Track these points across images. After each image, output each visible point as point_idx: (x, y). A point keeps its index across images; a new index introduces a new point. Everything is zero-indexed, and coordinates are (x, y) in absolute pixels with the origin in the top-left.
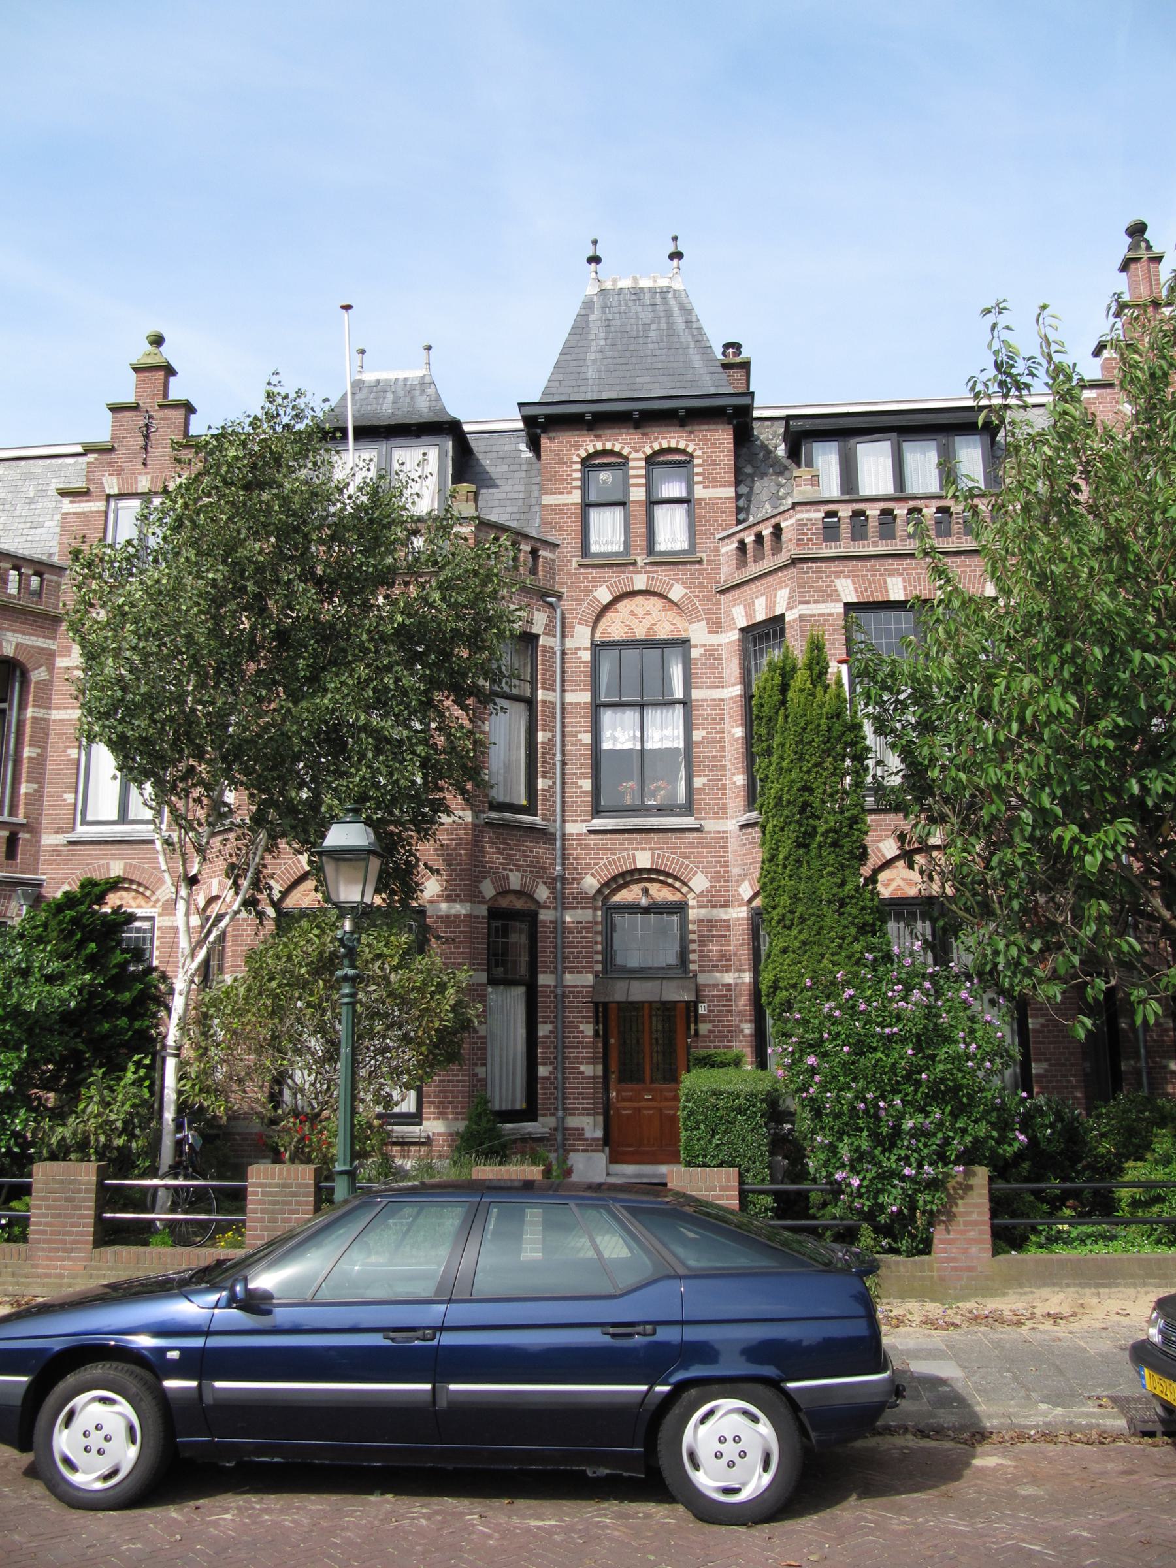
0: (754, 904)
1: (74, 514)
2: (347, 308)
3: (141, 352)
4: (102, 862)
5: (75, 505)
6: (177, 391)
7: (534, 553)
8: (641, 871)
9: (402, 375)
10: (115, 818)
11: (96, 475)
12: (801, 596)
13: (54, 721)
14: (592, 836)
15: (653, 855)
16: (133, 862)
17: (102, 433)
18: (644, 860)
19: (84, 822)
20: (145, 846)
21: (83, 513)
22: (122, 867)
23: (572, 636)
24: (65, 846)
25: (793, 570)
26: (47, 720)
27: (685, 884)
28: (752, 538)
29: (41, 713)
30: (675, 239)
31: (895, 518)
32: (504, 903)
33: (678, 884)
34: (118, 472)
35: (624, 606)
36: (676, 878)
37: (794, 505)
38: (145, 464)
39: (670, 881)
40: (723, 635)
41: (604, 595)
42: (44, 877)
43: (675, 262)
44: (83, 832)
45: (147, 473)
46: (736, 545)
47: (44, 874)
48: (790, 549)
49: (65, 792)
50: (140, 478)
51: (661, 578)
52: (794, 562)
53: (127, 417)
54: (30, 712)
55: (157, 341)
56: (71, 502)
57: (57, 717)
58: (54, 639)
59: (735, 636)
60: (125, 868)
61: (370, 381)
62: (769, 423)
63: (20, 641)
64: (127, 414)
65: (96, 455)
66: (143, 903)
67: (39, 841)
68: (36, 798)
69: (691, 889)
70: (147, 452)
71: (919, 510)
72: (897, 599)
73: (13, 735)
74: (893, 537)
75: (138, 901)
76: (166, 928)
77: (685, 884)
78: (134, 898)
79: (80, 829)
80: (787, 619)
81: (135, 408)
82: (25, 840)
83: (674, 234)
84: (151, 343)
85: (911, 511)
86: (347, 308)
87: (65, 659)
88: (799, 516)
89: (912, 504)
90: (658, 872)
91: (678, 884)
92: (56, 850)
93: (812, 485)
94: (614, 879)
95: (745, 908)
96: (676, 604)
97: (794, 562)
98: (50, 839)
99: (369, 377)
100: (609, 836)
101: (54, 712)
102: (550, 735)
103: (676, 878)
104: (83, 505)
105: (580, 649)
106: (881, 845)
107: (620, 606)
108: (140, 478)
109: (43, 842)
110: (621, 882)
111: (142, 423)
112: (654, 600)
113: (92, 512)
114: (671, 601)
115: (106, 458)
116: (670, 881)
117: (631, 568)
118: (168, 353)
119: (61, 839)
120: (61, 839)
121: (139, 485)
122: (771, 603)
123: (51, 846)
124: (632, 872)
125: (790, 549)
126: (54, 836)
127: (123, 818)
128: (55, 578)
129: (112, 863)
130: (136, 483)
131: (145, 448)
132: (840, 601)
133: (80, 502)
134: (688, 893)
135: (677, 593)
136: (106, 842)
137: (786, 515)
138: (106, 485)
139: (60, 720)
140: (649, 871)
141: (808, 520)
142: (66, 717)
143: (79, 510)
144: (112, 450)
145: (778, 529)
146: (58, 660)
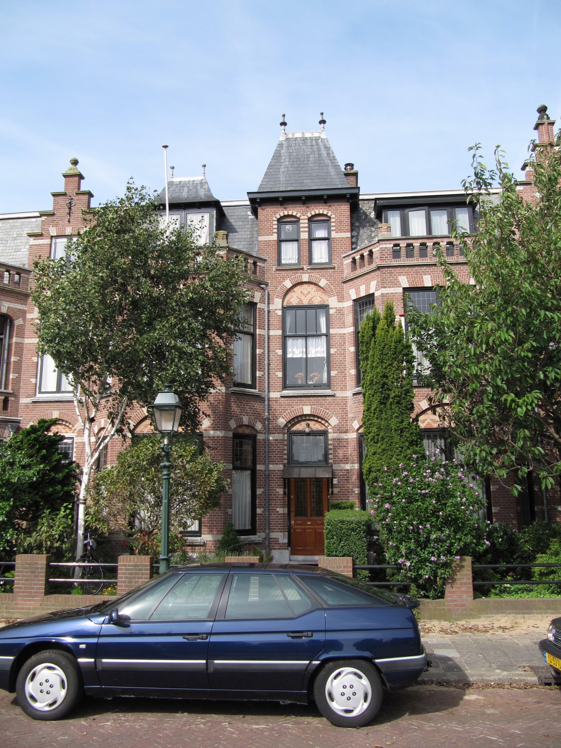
0: (360, 431)
1: (35, 245)
2: (166, 147)
3: (67, 168)
4: (49, 411)
5: (36, 241)
6: (84, 187)
7: (255, 264)
8: (306, 415)
9: (192, 179)
10: (55, 390)
11: (46, 227)
12: (382, 284)
13: (26, 344)
14: (283, 399)
15: (312, 408)
16: (63, 411)
17: (49, 207)
18: (307, 410)
19: (40, 392)
20: (69, 404)
21: (40, 245)
22: (58, 413)
23: (273, 304)
24: (31, 403)
25: (378, 272)
26: (22, 344)
27: (327, 422)
28: (359, 257)
29: (20, 340)
30: (322, 114)
31: (427, 247)
32: (240, 431)
33: (323, 422)
34: (56, 225)
35: (298, 289)
36: (323, 419)
37: (379, 241)
38: (69, 221)
39: (319, 420)
40: (345, 303)
41: (288, 284)
42: (21, 418)
43: (322, 125)
44: (40, 397)
45: (70, 226)
46: (351, 260)
47: (21, 417)
48: (377, 262)
49: (31, 378)
50: (67, 228)
51: (315, 276)
52: (379, 268)
53: (61, 199)
54: (14, 340)
55: (75, 162)
56: (34, 239)
57: (27, 342)
58: (26, 305)
59: (351, 303)
60: (60, 414)
61: (177, 182)
62: (367, 202)
63: (10, 306)
64: (61, 197)
65: (46, 217)
66: (68, 431)
67: (18, 401)
68: (17, 381)
69: (330, 424)
70: (70, 216)
71: (439, 243)
72: (428, 286)
73: (6, 351)
74: (426, 256)
75: (66, 430)
76: (79, 442)
77: (327, 422)
78: (64, 428)
79: (38, 395)
80: (375, 295)
81: (65, 194)
82: (12, 401)
83: (321, 112)
84: (72, 164)
85: (435, 244)
86: (166, 147)
87: (31, 315)
88: (381, 246)
89: (435, 240)
90: (314, 416)
91: (323, 422)
92: (27, 405)
93: (387, 231)
94: (293, 419)
95: (355, 433)
96: (322, 288)
97: (379, 268)
98: (24, 400)
99: (176, 180)
100: (290, 399)
101: (26, 340)
102: (262, 351)
103: (323, 419)
104: (40, 241)
105: (276, 310)
106: (420, 403)
107: (296, 289)
108: (67, 228)
109: (20, 402)
110: (296, 421)
111: (68, 202)
112: (312, 286)
113: (44, 244)
114: (320, 287)
115: (51, 218)
116: (319, 420)
117: (301, 271)
118: (80, 168)
119: (29, 400)
120: (29, 400)
121: (66, 232)
122: (368, 288)
123: (24, 403)
124: (301, 416)
125: (377, 262)
126: (26, 399)
127: (59, 390)
128: (26, 276)
129: (53, 412)
130: (65, 230)
131: (69, 214)
132: (401, 287)
133: (38, 239)
134: (328, 426)
135: (323, 283)
136: (51, 402)
137: (375, 246)
138: (50, 231)
139: (29, 344)
140: (310, 415)
141: (385, 248)
142: (32, 342)
143: (38, 243)
144: (53, 215)
145: (371, 252)
146: (28, 315)
